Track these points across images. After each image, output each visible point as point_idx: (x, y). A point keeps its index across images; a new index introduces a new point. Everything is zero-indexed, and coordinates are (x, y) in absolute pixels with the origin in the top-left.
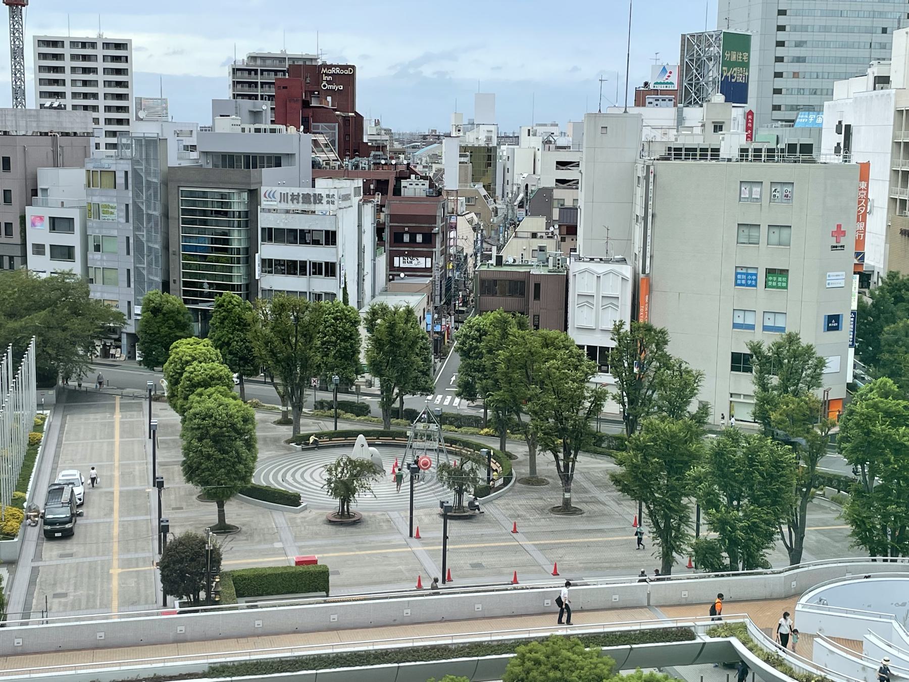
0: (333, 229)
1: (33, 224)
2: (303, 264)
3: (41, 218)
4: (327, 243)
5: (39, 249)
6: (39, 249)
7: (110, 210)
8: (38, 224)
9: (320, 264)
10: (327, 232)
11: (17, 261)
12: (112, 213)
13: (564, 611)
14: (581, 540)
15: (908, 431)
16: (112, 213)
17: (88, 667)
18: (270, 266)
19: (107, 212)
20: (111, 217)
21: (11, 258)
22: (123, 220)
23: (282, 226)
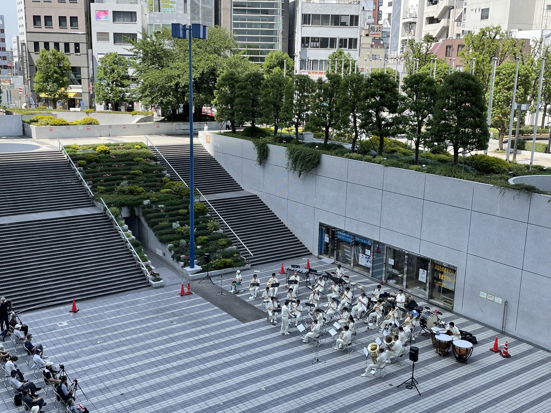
0: (357, 14)
1: (98, 17)
2: (333, 40)
3: (105, 12)
4: (351, 24)
5: (103, 36)
6: (103, 36)
7: (170, 4)
8: (103, 17)
9: (346, 40)
10: (352, 16)
11: (83, 48)
12: (172, 7)
13: (208, 277)
14: (68, 213)
15: (550, 120)
16: (172, 7)
17: (243, 407)
18: (308, 42)
19: (167, 6)
20: (170, 10)
21: (77, 45)
22: (181, 12)
23: (318, 12)
